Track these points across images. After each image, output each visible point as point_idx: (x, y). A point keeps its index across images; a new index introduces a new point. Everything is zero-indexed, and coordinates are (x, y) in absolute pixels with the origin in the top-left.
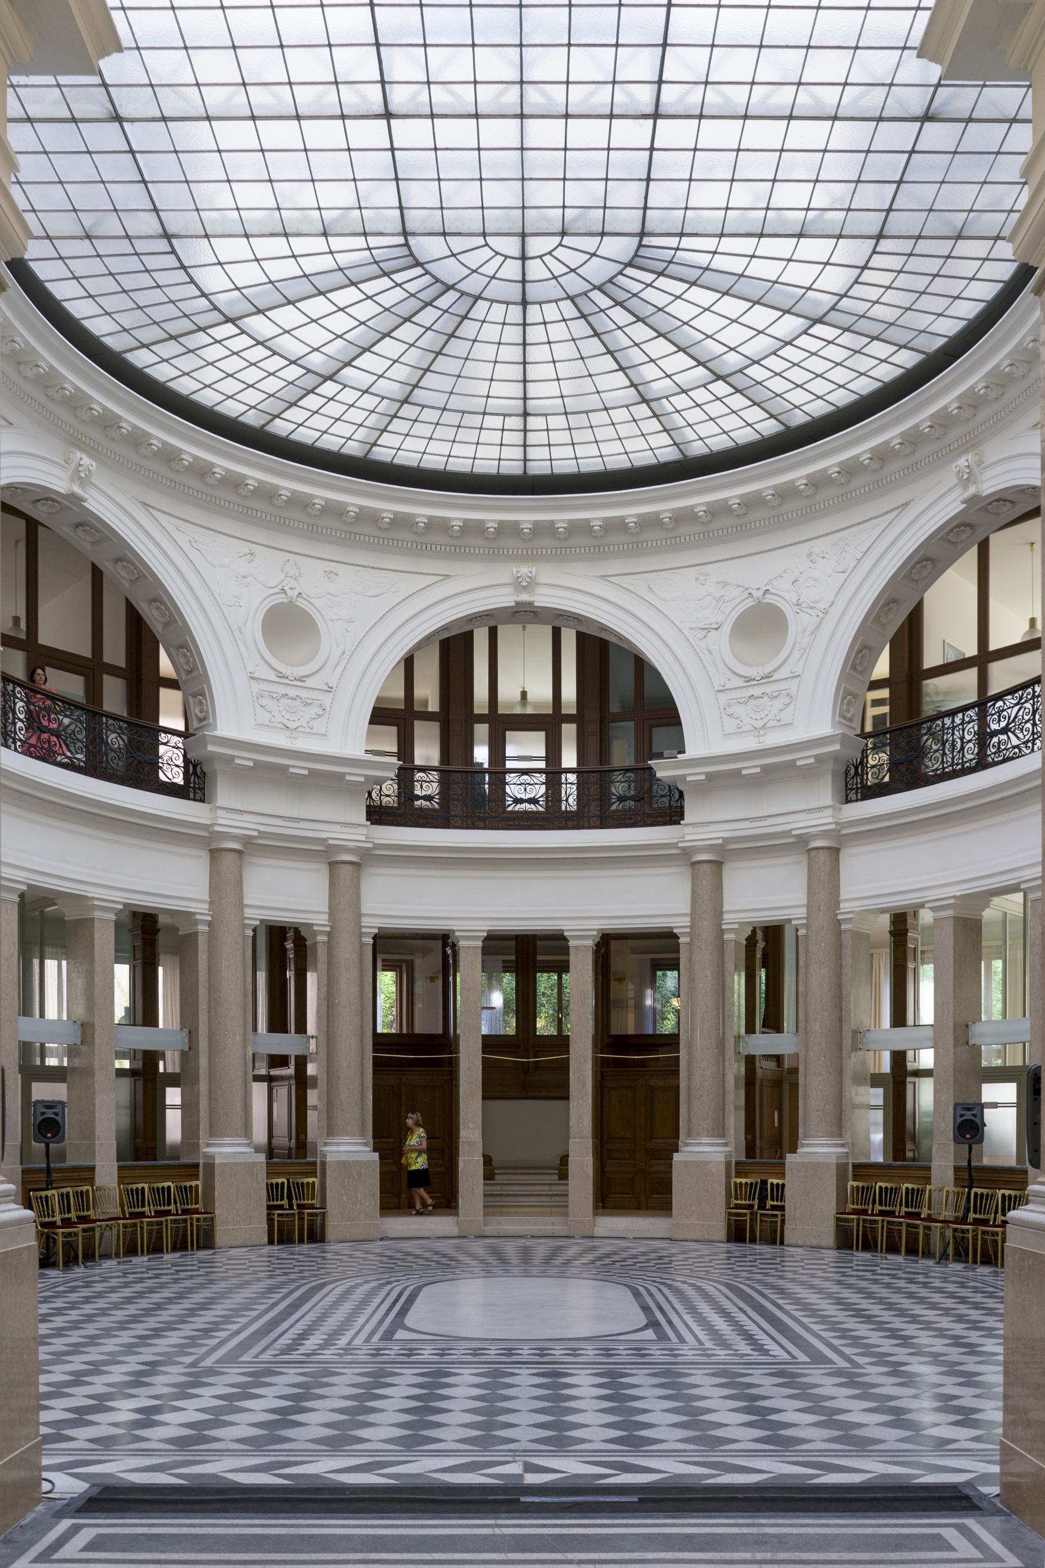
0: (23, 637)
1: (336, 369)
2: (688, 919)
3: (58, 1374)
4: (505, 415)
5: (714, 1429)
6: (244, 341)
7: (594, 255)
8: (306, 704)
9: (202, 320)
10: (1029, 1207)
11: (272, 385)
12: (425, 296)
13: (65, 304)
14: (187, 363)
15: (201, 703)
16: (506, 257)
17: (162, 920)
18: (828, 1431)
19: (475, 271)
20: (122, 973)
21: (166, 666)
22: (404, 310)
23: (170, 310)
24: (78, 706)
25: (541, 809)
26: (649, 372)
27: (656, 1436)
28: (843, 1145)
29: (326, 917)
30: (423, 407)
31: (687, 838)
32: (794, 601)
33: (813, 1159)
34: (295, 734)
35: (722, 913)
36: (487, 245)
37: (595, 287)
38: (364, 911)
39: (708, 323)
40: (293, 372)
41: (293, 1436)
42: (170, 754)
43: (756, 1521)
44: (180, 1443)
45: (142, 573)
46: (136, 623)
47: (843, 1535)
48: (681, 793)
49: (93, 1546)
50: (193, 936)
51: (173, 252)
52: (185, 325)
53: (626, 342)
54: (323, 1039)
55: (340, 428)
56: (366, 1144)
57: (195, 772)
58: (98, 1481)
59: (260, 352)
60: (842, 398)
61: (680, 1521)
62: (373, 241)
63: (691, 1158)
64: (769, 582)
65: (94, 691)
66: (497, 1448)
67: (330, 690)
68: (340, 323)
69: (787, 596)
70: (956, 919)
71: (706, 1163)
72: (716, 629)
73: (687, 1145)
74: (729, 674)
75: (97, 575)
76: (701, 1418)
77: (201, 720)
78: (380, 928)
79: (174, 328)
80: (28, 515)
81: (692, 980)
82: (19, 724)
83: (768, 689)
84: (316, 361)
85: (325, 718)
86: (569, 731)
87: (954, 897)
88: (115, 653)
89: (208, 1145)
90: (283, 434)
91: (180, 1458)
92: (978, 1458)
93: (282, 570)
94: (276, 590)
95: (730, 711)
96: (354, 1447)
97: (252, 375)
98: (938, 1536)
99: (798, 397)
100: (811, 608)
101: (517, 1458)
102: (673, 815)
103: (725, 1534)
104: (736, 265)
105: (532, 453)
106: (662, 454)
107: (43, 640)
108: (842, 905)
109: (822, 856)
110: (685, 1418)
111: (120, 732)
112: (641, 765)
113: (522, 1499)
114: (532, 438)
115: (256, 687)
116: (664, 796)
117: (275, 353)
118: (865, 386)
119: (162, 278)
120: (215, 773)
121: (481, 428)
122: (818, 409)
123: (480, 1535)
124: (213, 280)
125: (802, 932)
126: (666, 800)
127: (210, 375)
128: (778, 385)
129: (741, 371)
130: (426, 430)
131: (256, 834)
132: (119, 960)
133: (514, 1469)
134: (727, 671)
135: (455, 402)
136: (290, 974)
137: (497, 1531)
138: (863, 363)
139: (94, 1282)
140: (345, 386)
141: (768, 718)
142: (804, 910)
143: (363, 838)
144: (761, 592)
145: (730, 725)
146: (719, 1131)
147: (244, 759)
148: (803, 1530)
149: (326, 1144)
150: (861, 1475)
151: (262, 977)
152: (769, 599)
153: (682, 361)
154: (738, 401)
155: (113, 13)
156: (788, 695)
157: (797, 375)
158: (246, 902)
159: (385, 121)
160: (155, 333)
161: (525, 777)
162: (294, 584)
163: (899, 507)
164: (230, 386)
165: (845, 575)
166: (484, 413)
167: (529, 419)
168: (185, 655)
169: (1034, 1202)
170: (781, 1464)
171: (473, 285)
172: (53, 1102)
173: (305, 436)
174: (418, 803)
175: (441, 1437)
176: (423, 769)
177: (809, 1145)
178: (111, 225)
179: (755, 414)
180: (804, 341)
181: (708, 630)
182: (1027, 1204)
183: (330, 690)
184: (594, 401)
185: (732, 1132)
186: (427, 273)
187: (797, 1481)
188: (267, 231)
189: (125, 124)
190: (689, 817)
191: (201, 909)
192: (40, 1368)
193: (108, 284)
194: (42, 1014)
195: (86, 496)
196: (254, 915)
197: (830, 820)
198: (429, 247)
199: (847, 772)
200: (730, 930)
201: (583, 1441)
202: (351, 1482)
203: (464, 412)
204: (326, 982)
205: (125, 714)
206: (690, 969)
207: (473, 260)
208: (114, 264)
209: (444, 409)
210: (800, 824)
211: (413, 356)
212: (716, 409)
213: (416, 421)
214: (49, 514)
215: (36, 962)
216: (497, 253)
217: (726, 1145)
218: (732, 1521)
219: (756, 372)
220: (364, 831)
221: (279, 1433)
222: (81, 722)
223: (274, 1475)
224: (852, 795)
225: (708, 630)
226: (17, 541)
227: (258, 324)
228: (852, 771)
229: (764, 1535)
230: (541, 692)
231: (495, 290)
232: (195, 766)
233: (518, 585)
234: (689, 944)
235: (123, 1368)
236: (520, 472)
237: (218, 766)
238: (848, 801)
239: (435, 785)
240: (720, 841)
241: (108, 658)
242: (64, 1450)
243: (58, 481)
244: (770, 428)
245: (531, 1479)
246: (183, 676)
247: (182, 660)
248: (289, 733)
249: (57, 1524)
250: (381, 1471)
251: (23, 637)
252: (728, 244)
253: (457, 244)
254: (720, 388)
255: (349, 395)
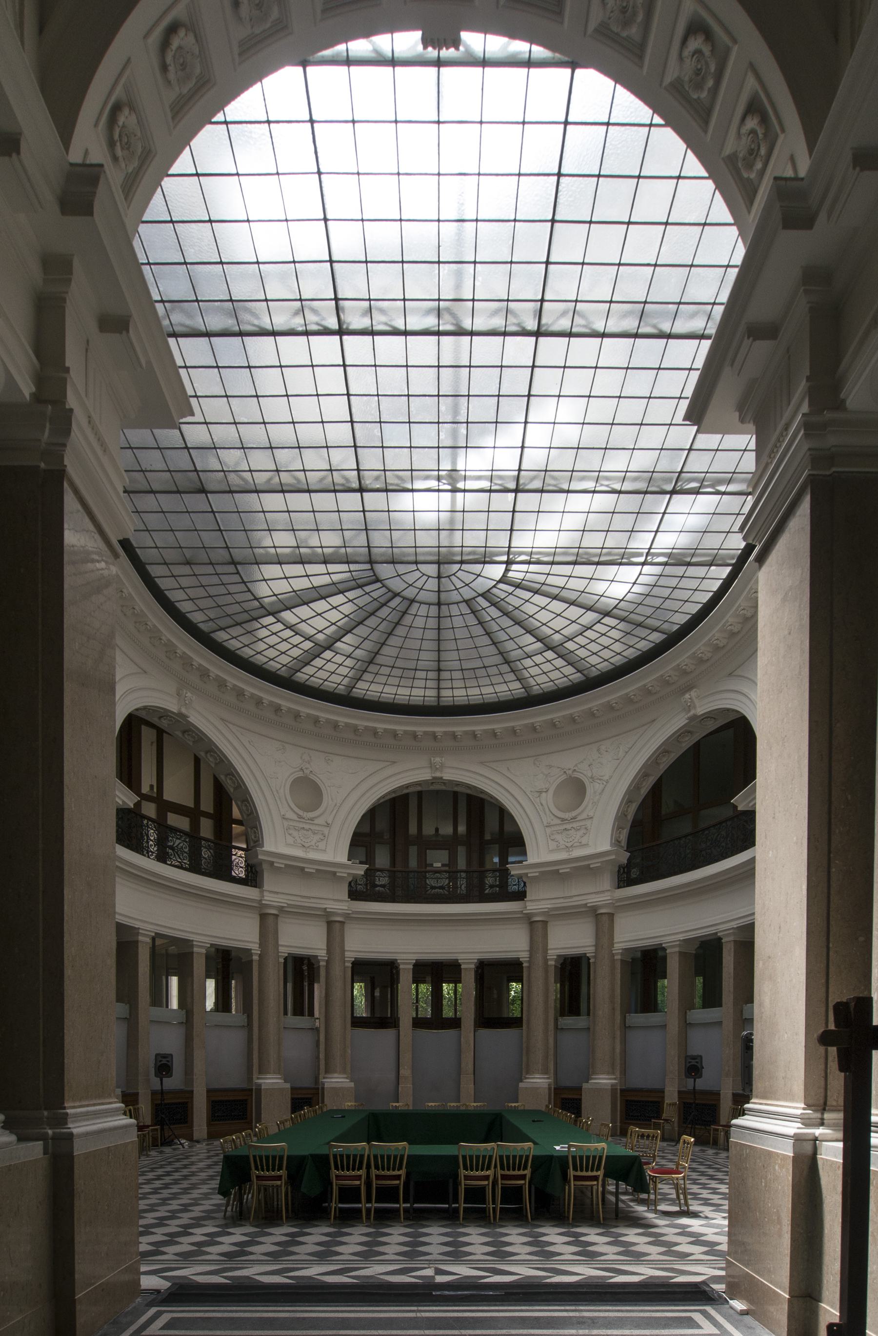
0: (155, 795)
1: (331, 643)
2: (528, 953)
3: (149, 1218)
4: (427, 671)
5: (548, 1246)
6: (280, 626)
7: (479, 575)
8: (314, 833)
9: (254, 614)
10: (746, 1117)
11: (296, 652)
12: (382, 600)
13: (177, 604)
14: (246, 640)
15: (255, 833)
16: (429, 577)
17: (233, 954)
18: (616, 1247)
19: (411, 585)
20: (211, 985)
21: (236, 813)
22: (370, 609)
23: (237, 608)
24: (185, 833)
25: (446, 892)
26: (510, 645)
27: (514, 1251)
28: (615, 1079)
29: (325, 952)
30: (381, 665)
31: (528, 908)
32: (590, 775)
33: (535, 1085)
34: (308, 850)
35: (547, 950)
36: (418, 569)
37: (480, 595)
38: (346, 949)
39: (544, 616)
40: (308, 645)
41: (297, 1251)
42: (237, 860)
43: (577, 1308)
44: (229, 1255)
45: (222, 761)
46: (219, 789)
47: (632, 1317)
48: (525, 883)
49: (167, 1326)
50: (251, 962)
51: (238, 573)
52: (246, 616)
53: (497, 628)
54: (323, 1019)
55: (334, 678)
56: (347, 1078)
57: (251, 871)
58: (177, 1281)
59: (288, 633)
60: (618, 660)
61: (531, 1308)
62: (353, 567)
63: (529, 1086)
64: (576, 765)
65: (195, 825)
66: (419, 1259)
67: (328, 825)
68: (334, 616)
69: (585, 772)
70: (680, 953)
71: (537, 1088)
72: (546, 792)
73: (526, 1078)
74: (553, 817)
75: (197, 761)
76: (540, 1239)
77: (255, 842)
78: (355, 958)
79: (239, 618)
80: (158, 727)
81: (529, 987)
82: (151, 843)
83: (575, 825)
84: (320, 637)
85: (325, 842)
86: (462, 851)
87: (679, 940)
88: (207, 804)
89: (258, 1078)
90: (302, 681)
91: (229, 1266)
92: (708, 1265)
93: (301, 758)
94: (298, 769)
95: (553, 837)
96: (334, 1258)
97: (284, 646)
98: (690, 1318)
99: (594, 660)
100: (600, 779)
101: (431, 1265)
102: (520, 896)
103: (558, 1317)
104: (561, 581)
105: (444, 693)
106: (516, 694)
107: (166, 797)
108: (615, 945)
109: (605, 919)
110: (530, 1239)
111: (208, 848)
112: (503, 868)
113: (434, 1293)
114: (443, 684)
115: (286, 823)
116: (515, 885)
117: (297, 634)
118: (631, 653)
119: (233, 589)
120: (263, 871)
121: (414, 678)
122: (605, 667)
123: (408, 1317)
124: (262, 590)
125: (592, 961)
126: (516, 887)
127: (261, 646)
128: (582, 653)
129: (561, 644)
130: (383, 679)
131: (286, 905)
132: (208, 976)
133: (429, 1272)
134: (551, 815)
135: (399, 663)
136: (306, 984)
137: (419, 1315)
138: (632, 641)
139: (192, 1156)
140: (337, 653)
141: (576, 840)
142: (593, 948)
143: (346, 908)
144: (570, 772)
145: (553, 845)
146: (545, 1071)
147: (279, 863)
148: (606, 1314)
149: (324, 1078)
150: (638, 1276)
151: (290, 986)
152: (576, 775)
153: (530, 639)
154: (560, 662)
155: (143, 267)
156: (586, 828)
157: (594, 647)
158: (280, 943)
159: (338, 337)
160: (228, 621)
161: (438, 875)
162: (308, 766)
163: (648, 723)
164: (271, 653)
165: (618, 761)
166: (416, 670)
167: (441, 673)
168: (246, 806)
169: (748, 1115)
170: (589, 1269)
171: (410, 593)
172: (165, 1054)
173: (315, 682)
174: (377, 889)
175: (386, 1251)
176: (381, 870)
177: (595, 1079)
178: (202, 556)
179: (569, 670)
180: (598, 627)
181: (540, 792)
182: (743, 1115)
183: (328, 825)
184: (478, 664)
185: (552, 1071)
186: (384, 586)
187: (600, 1281)
188: (291, 560)
189: (208, 495)
190: (528, 897)
191: (255, 947)
192: (141, 1213)
193: (201, 592)
194: (167, 1006)
195: (189, 714)
196: (284, 951)
197: (609, 898)
198: (385, 571)
199: (619, 871)
200: (551, 959)
201: (471, 1254)
202: (330, 1281)
203: (404, 669)
204: (324, 987)
205: (213, 838)
206: (529, 981)
207: (410, 579)
208: (204, 580)
209: (393, 667)
210: (593, 900)
211: (375, 636)
212: (547, 667)
213: (377, 674)
214: (168, 725)
215: (164, 978)
216: (424, 574)
217: (548, 1078)
218: (563, 1308)
219: (570, 645)
220: (347, 904)
221: (289, 1249)
222: (186, 842)
223: (284, 1277)
224: (621, 884)
225: (540, 792)
226: (152, 743)
227: (287, 615)
228: (622, 870)
229: (583, 1317)
230: (447, 830)
231: (422, 597)
232: (251, 868)
233: (432, 766)
234: (529, 967)
235: (201, 1208)
236: (436, 704)
237: (265, 866)
238: (619, 887)
239: (387, 879)
240: (546, 910)
241: (203, 807)
242: (159, 1260)
243: (172, 705)
244: (577, 677)
245: (440, 1279)
246: (245, 817)
247: (244, 808)
248: (305, 849)
249: (148, 1310)
250: (349, 1274)
251: (155, 795)
252: (556, 569)
253: (401, 569)
254: (550, 655)
255: (339, 659)
